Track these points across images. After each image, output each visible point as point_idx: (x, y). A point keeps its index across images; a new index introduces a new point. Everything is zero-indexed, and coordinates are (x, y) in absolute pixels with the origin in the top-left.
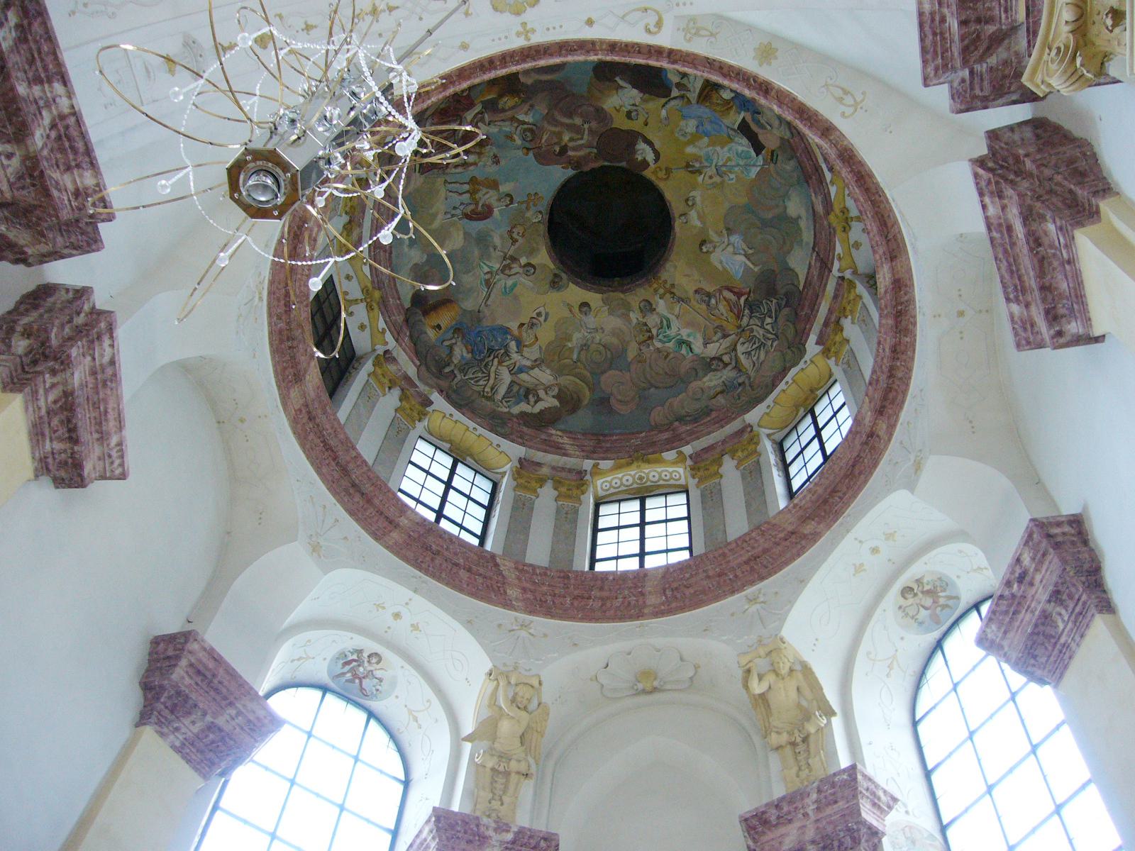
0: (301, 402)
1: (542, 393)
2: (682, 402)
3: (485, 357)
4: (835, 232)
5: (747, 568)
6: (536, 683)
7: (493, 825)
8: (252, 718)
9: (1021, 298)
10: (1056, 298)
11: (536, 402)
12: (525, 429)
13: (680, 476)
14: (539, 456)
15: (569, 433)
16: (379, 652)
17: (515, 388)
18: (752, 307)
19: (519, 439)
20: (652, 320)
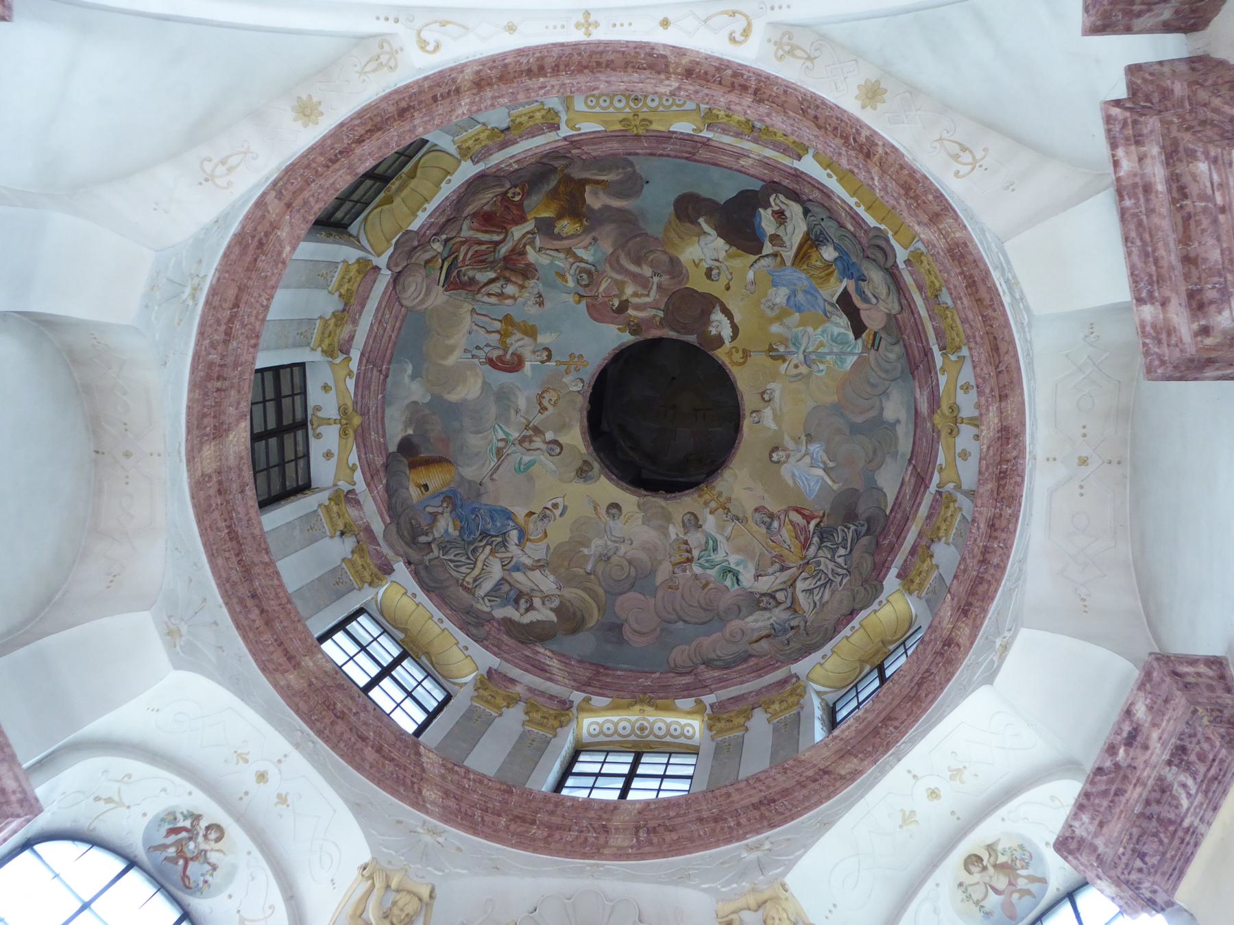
0: (215, 466)
1: (537, 602)
2: (714, 643)
3: (475, 540)
4: (939, 437)
5: (757, 814)
6: (425, 893)
9: (1156, 294)
10: (1204, 275)
11: (527, 610)
12: (505, 638)
13: (694, 733)
14: (515, 672)
15: (563, 657)
16: (223, 825)
17: (506, 588)
18: (824, 534)
19: (496, 648)
20: (695, 539)
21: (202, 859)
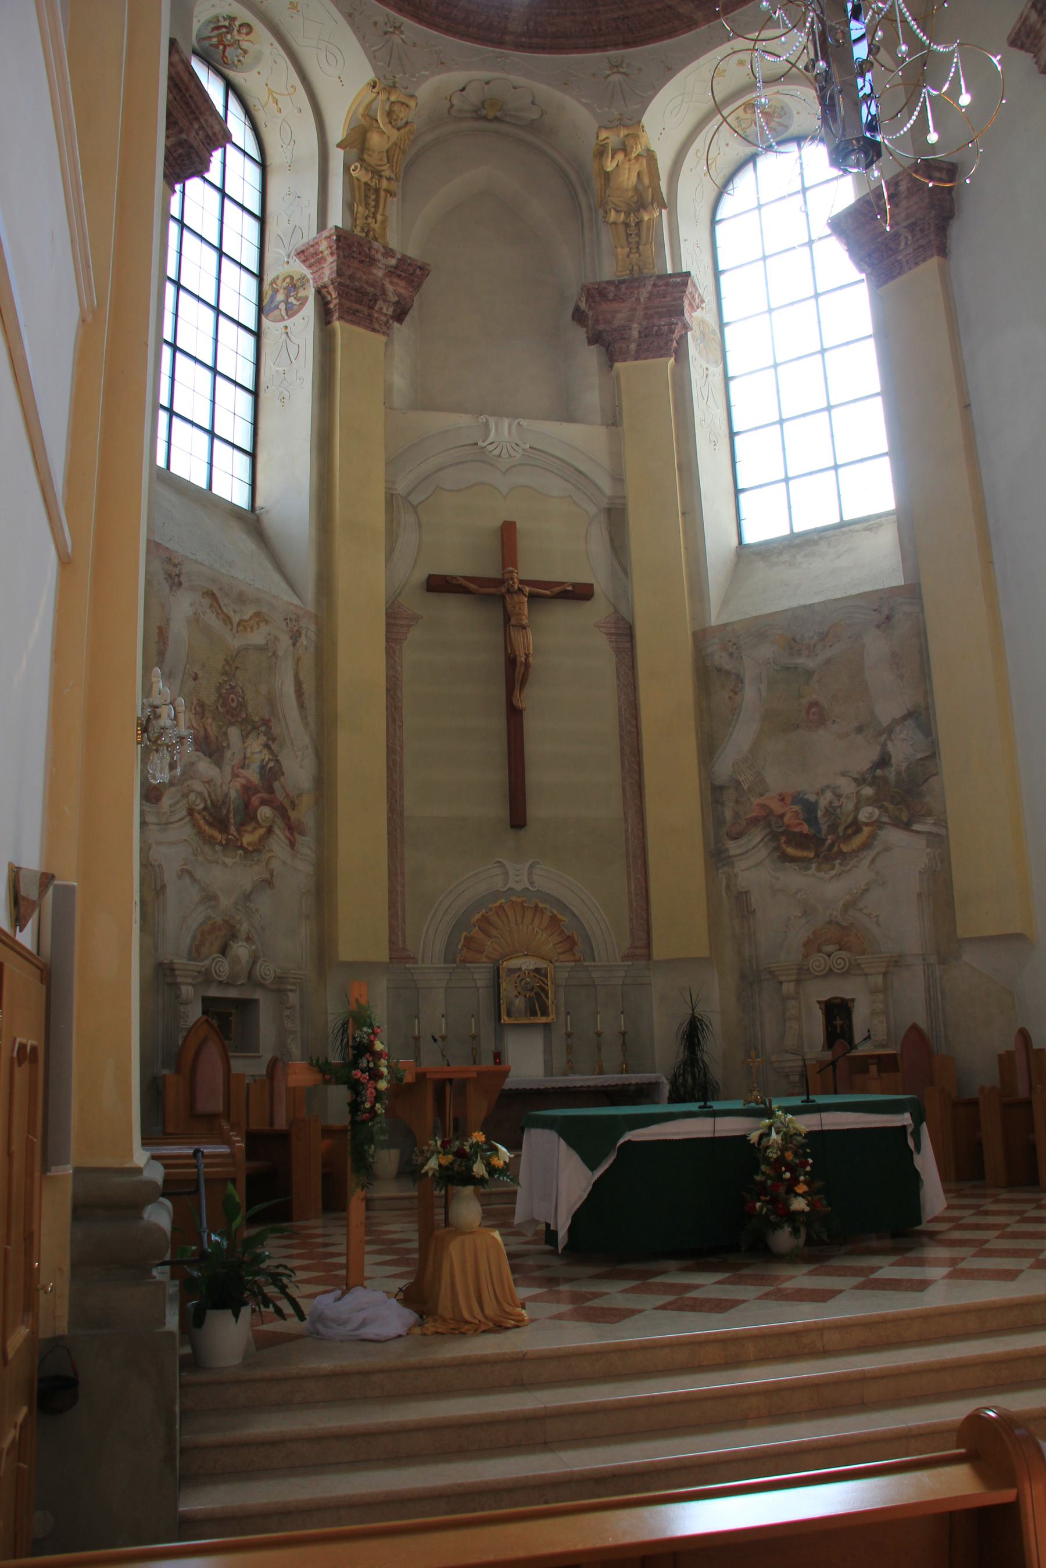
7: (382, 250)
8: (210, 133)
21: (235, 46)
